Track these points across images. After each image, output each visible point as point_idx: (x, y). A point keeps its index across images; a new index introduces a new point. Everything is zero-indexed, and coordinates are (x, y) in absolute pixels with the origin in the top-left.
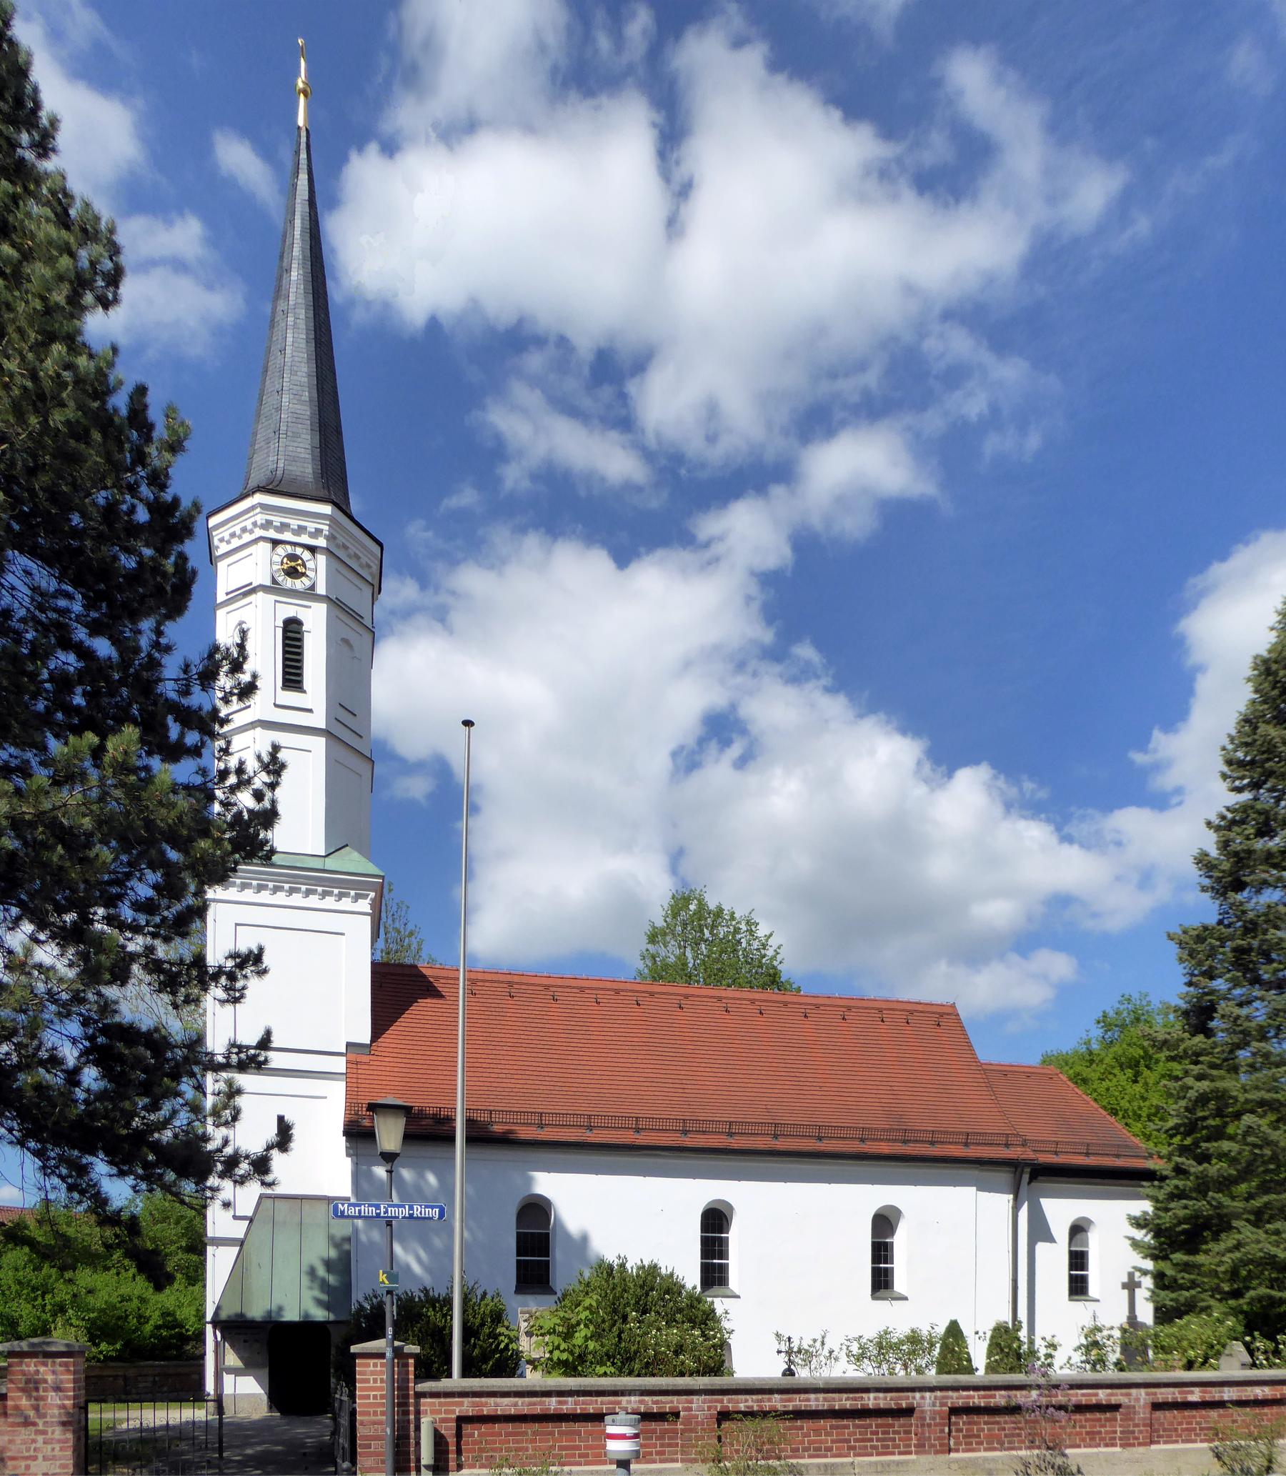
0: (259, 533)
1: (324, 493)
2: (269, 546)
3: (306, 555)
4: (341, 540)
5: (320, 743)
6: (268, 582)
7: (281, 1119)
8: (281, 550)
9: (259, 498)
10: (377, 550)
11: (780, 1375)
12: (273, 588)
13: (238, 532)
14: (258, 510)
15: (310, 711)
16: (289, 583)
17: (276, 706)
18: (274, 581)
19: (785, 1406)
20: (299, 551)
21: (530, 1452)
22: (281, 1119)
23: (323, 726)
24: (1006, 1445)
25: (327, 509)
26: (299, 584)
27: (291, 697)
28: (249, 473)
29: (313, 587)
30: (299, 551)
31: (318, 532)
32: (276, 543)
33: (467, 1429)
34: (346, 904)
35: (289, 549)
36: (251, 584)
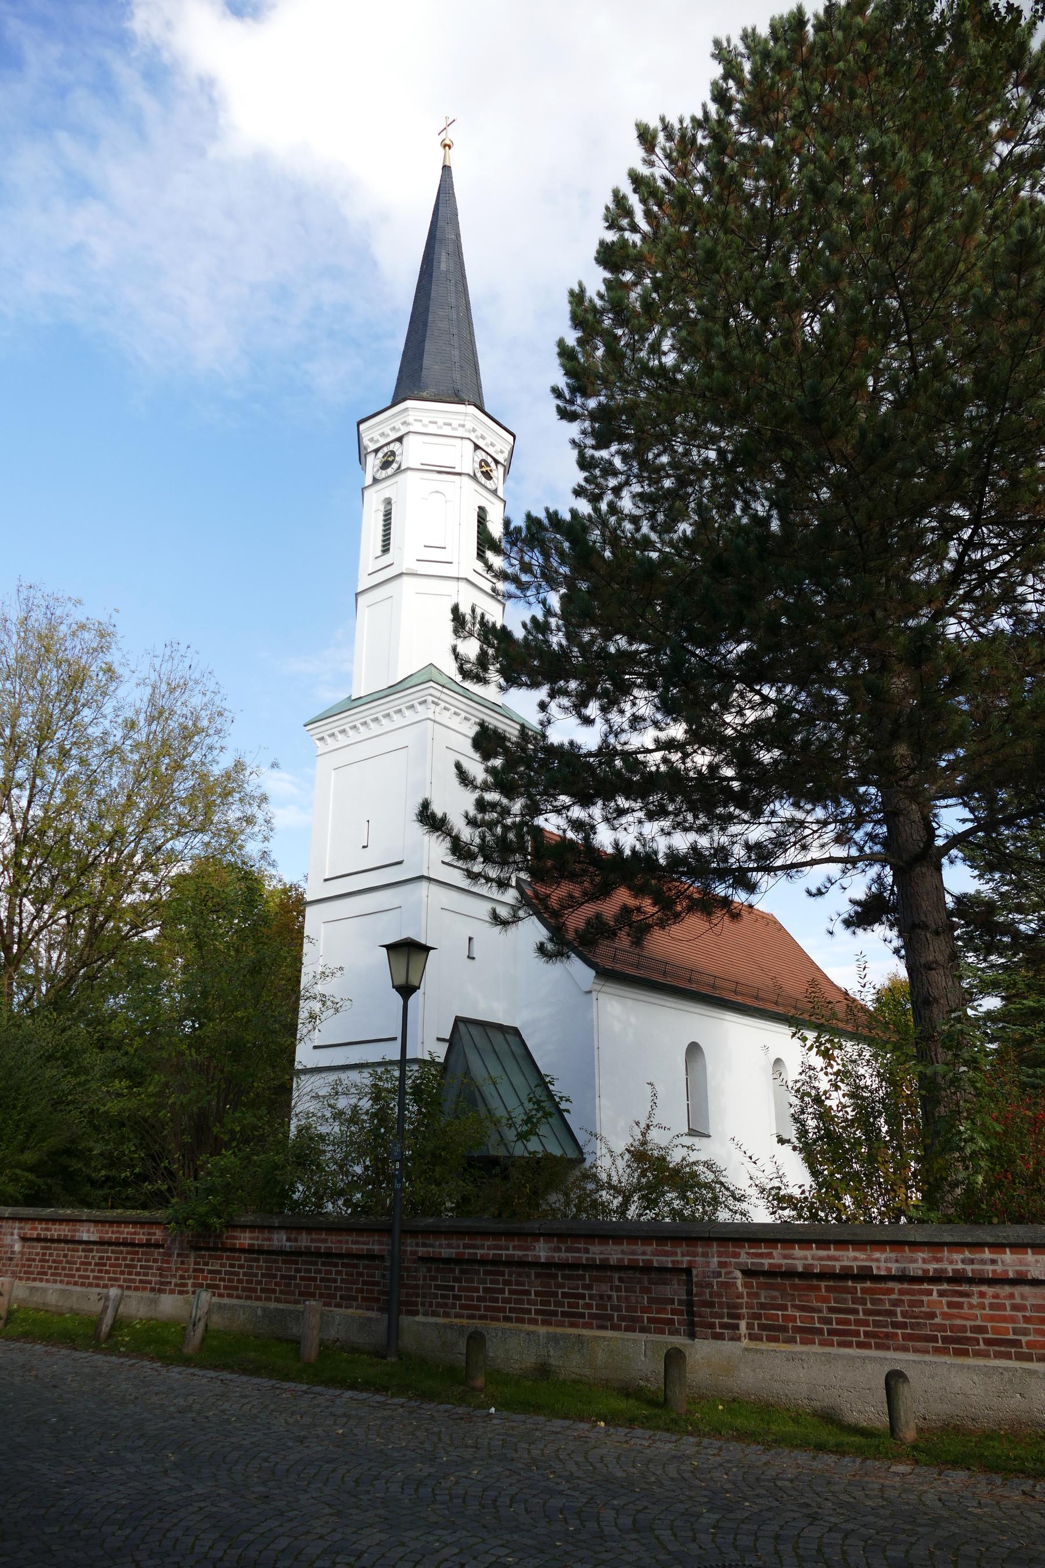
2: (472, 446)
3: (493, 465)
6: (472, 474)
8: (480, 455)
12: (474, 477)
20: (489, 460)
30: (489, 460)
32: (477, 447)
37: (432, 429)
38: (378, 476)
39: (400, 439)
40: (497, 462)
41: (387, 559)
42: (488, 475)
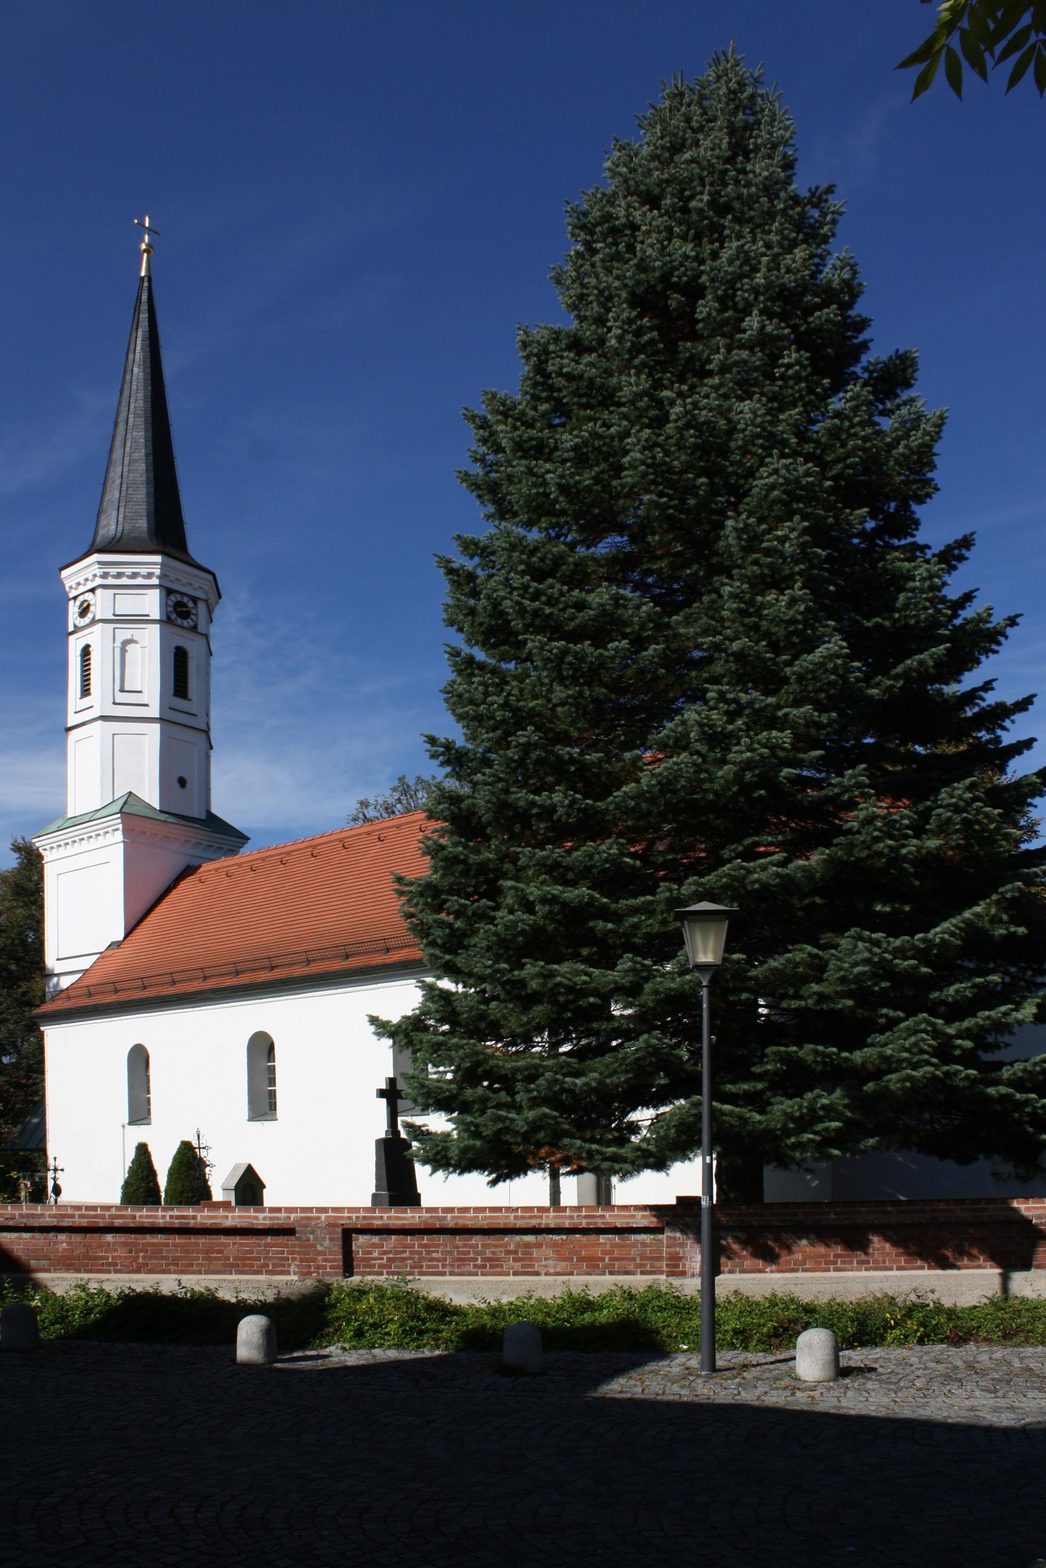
0: (99, 581)
1: (152, 548)
3: (191, 604)
4: (173, 576)
5: (157, 727)
7: (1033, 740)
8: (173, 598)
9: (95, 557)
10: (211, 578)
11: (113, 1196)
13: (82, 582)
14: (97, 566)
15: (147, 705)
16: (179, 621)
17: (114, 703)
19: (431, 1240)
20: (185, 600)
21: (320, 1258)
22: (1033, 740)
23: (158, 716)
24: (424, 1269)
25: (158, 558)
26: (185, 623)
27: (180, 703)
28: (96, 533)
31: (150, 576)
33: (360, 1241)
34: (101, 841)
35: (179, 597)
36: (148, 615)
37: (139, 581)
38: (77, 623)
39: (93, 590)
40: (195, 600)
41: (87, 701)
42: (185, 615)
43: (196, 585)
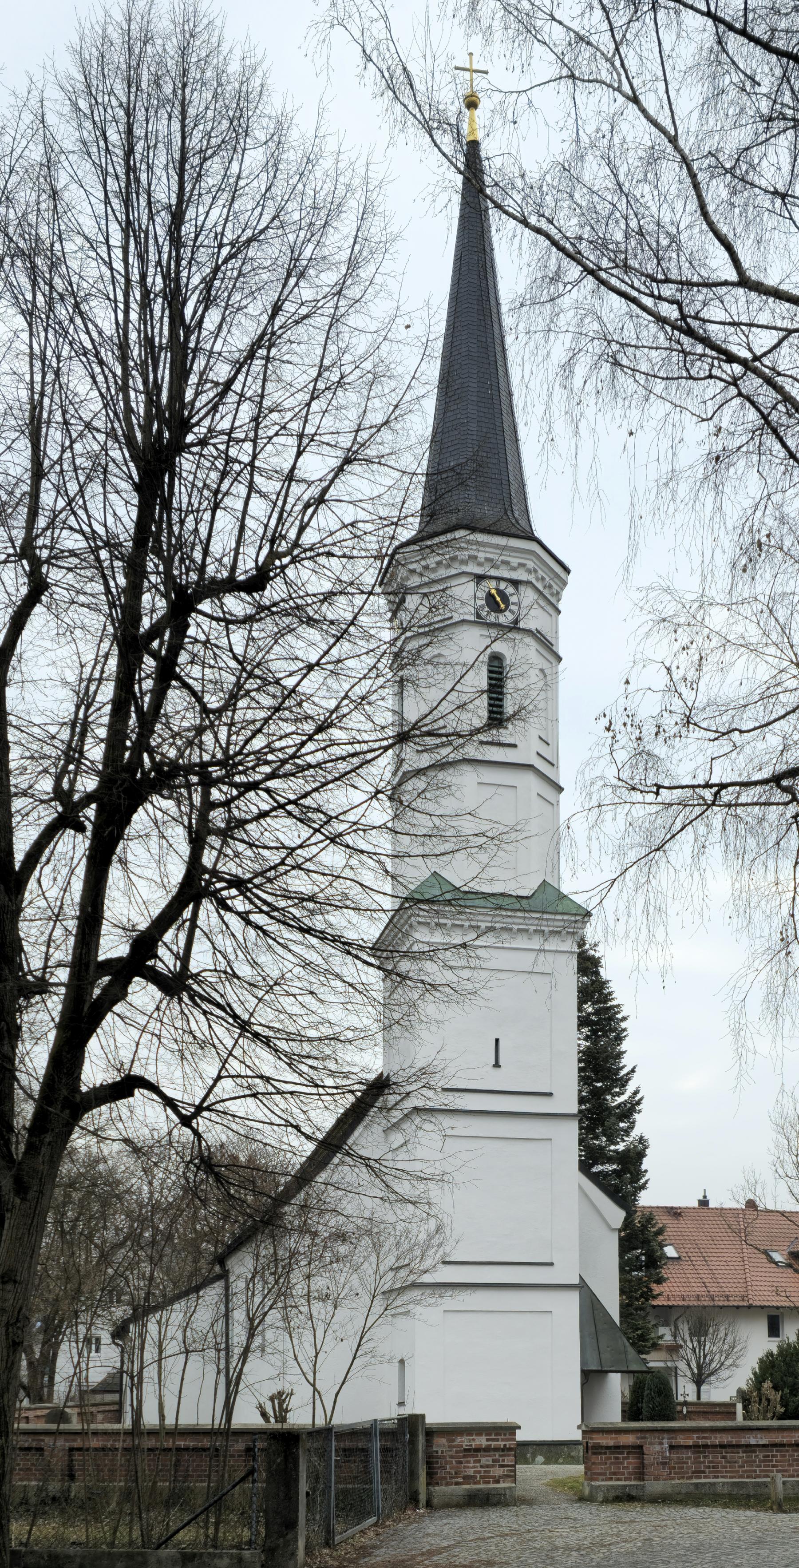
3: (510, 590)
18: (478, 616)
29: (516, 622)
32: (480, 578)
35: (493, 584)
43: (515, 562)
